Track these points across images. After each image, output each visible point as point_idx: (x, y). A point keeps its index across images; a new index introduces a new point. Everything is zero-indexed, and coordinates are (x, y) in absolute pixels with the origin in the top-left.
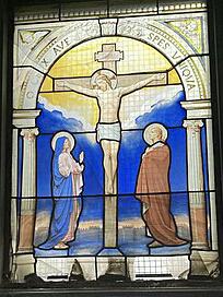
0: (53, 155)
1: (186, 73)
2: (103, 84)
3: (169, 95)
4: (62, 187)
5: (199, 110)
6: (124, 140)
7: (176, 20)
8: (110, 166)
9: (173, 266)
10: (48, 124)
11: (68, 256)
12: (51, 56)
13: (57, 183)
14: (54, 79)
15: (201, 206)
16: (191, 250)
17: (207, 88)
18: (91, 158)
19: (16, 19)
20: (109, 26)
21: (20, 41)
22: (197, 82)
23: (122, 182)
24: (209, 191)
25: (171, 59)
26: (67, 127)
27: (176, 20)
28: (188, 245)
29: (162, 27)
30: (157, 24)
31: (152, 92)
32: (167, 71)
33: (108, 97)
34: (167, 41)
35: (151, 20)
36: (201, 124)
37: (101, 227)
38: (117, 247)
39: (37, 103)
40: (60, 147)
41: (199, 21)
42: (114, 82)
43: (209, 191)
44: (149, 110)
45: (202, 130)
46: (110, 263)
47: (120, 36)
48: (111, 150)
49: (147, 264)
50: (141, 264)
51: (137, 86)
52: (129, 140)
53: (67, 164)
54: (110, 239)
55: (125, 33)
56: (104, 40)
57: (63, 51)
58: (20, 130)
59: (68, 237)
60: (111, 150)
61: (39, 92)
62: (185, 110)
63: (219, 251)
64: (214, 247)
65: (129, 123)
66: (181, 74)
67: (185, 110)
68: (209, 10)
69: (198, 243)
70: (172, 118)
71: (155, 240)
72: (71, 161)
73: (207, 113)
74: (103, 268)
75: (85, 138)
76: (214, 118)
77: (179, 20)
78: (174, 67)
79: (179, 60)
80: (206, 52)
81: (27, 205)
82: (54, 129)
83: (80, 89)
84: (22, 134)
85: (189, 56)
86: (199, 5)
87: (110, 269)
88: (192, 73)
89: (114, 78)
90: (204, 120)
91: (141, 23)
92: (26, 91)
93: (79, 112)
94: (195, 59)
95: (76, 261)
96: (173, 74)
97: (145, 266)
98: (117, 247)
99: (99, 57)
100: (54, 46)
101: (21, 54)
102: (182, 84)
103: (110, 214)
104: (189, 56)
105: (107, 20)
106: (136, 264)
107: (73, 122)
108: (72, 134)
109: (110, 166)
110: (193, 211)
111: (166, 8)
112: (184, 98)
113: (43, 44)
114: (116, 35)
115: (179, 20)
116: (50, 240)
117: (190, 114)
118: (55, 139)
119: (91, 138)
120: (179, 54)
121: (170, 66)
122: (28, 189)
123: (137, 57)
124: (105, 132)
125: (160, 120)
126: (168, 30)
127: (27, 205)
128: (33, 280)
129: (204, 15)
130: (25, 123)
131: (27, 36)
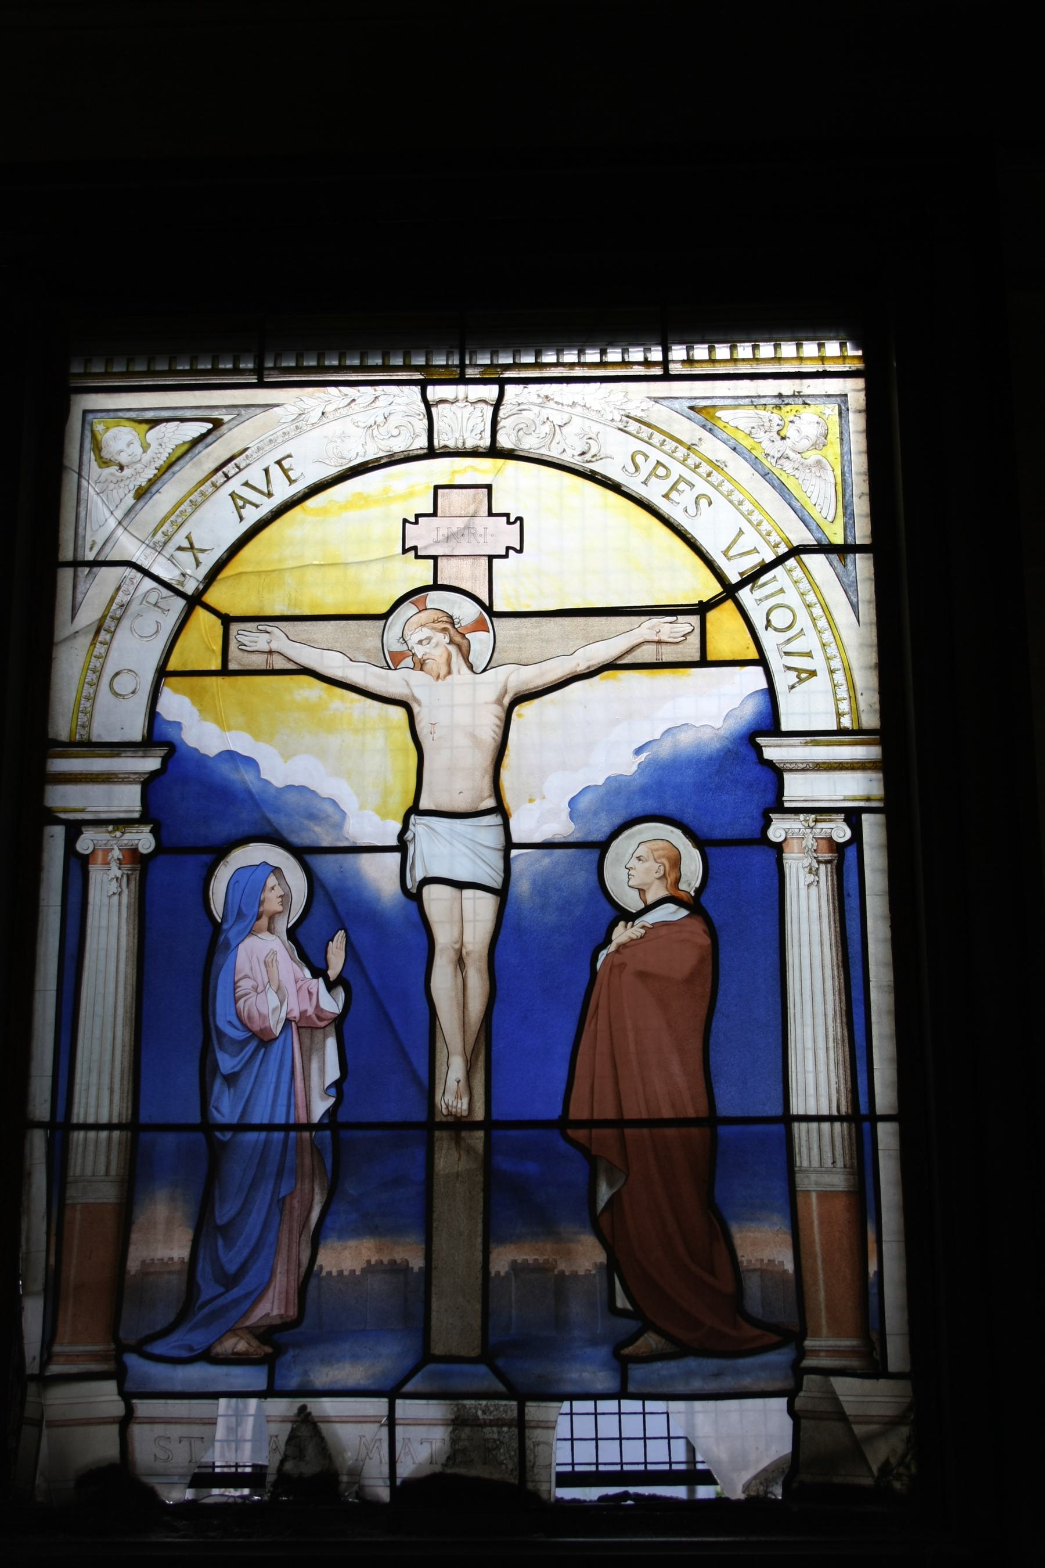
0: (215, 943)
1: (780, 619)
2: (436, 647)
3: (709, 707)
4: (246, 1084)
5: (829, 784)
6: (522, 887)
7: (737, 402)
8: (456, 995)
9: (740, 1438)
10: (198, 813)
11: (270, 1392)
12: (217, 525)
13: (227, 1063)
14: (227, 620)
15: (838, 1181)
16: (798, 1372)
17: (866, 681)
18: (371, 946)
19: (76, 368)
20: (462, 412)
21: (90, 457)
22: (822, 652)
23: (560, 1123)
24: (874, 1118)
25: (721, 561)
26: (281, 822)
27: (737, 402)
28: (782, 1357)
29: (687, 429)
30: (659, 414)
31: (338, 645)
32: (702, 609)
33: (459, 708)
34: (702, 487)
35: (636, 396)
36: (842, 832)
37: (417, 1263)
38: (487, 1356)
39: (152, 715)
40: (248, 914)
41: (831, 410)
42: (480, 643)
43: (874, 1118)
44: (627, 765)
45: (843, 860)
46: (457, 1423)
47: (510, 455)
48: (462, 923)
49: (608, 1426)
50: (584, 1427)
51: (581, 662)
52: (543, 887)
53: (269, 980)
54: (453, 1324)
55: (529, 444)
56: (441, 470)
57: (268, 505)
58: (74, 829)
59: (271, 1307)
60: (462, 923)
61: (163, 673)
62: (776, 772)
63: (920, 1373)
64: (896, 1352)
65: (540, 818)
66: (759, 624)
67: (776, 772)
68: (872, 375)
69: (824, 1344)
70: (725, 797)
71: (648, 1326)
72: (290, 969)
73: (854, 788)
74: (424, 1438)
75: (357, 874)
76: (893, 806)
77: (754, 401)
78: (730, 591)
79: (749, 563)
80: (862, 534)
81: (95, 1159)
82: (221, 831)
83: (333, 664)
84: (85, 844)
85: (795, 551)
86: (832, 348)
87: (456, 1453)
88: (803, 620)
89: (479, 626)
90: (852, 816)
91: (584, 407)
92: (110, 670)
93: (330, 761)
94: (816, 562)
95: (304, 1417)
96: (725, 626)
97: (598, 1436)
98: (487, 1356)
99: (421, 536)
100: (235, 485)
101: (102, 513)
102: (762, 661)
103: (458, 1215)
104: (795, 551)
105: (461, 390)
106: (563, 1428)
107: (308, 802)
108: (301, 853)
109: (456, 995)
110: (813, 1210)
111: (701, 352)
112: (769, 723)
113: (191, 473)
114: (494, 452)
115: (754, 401)
116: (197, 1301)
117: (797, 789)
118: (223, 876)
119: (380, 874)
120: (751, 539)
121: (716, 589)
122: (100, 1090)
123: (578, 548)
124: (441, 849)
125: (671, 808)
126: (713, 448)
127: (95, 1159)
128: (119, 1485)
129: (854, 389)
130: (105, 798)
131: (120, 440)
